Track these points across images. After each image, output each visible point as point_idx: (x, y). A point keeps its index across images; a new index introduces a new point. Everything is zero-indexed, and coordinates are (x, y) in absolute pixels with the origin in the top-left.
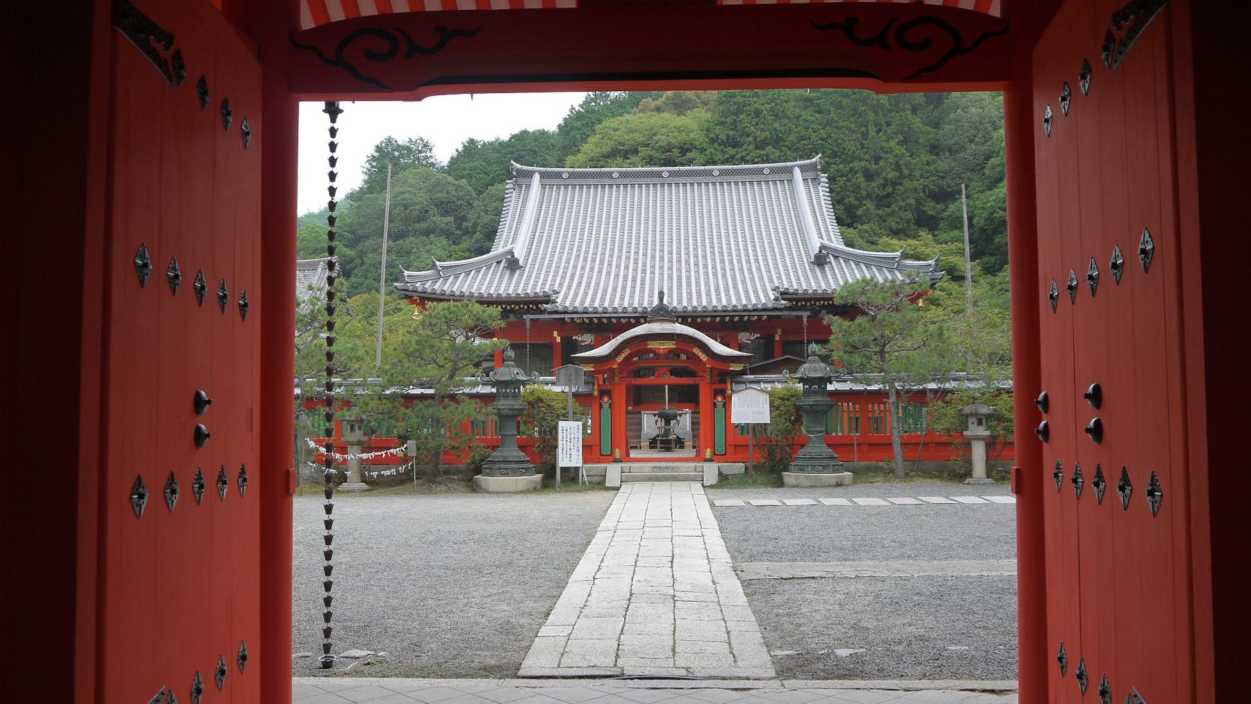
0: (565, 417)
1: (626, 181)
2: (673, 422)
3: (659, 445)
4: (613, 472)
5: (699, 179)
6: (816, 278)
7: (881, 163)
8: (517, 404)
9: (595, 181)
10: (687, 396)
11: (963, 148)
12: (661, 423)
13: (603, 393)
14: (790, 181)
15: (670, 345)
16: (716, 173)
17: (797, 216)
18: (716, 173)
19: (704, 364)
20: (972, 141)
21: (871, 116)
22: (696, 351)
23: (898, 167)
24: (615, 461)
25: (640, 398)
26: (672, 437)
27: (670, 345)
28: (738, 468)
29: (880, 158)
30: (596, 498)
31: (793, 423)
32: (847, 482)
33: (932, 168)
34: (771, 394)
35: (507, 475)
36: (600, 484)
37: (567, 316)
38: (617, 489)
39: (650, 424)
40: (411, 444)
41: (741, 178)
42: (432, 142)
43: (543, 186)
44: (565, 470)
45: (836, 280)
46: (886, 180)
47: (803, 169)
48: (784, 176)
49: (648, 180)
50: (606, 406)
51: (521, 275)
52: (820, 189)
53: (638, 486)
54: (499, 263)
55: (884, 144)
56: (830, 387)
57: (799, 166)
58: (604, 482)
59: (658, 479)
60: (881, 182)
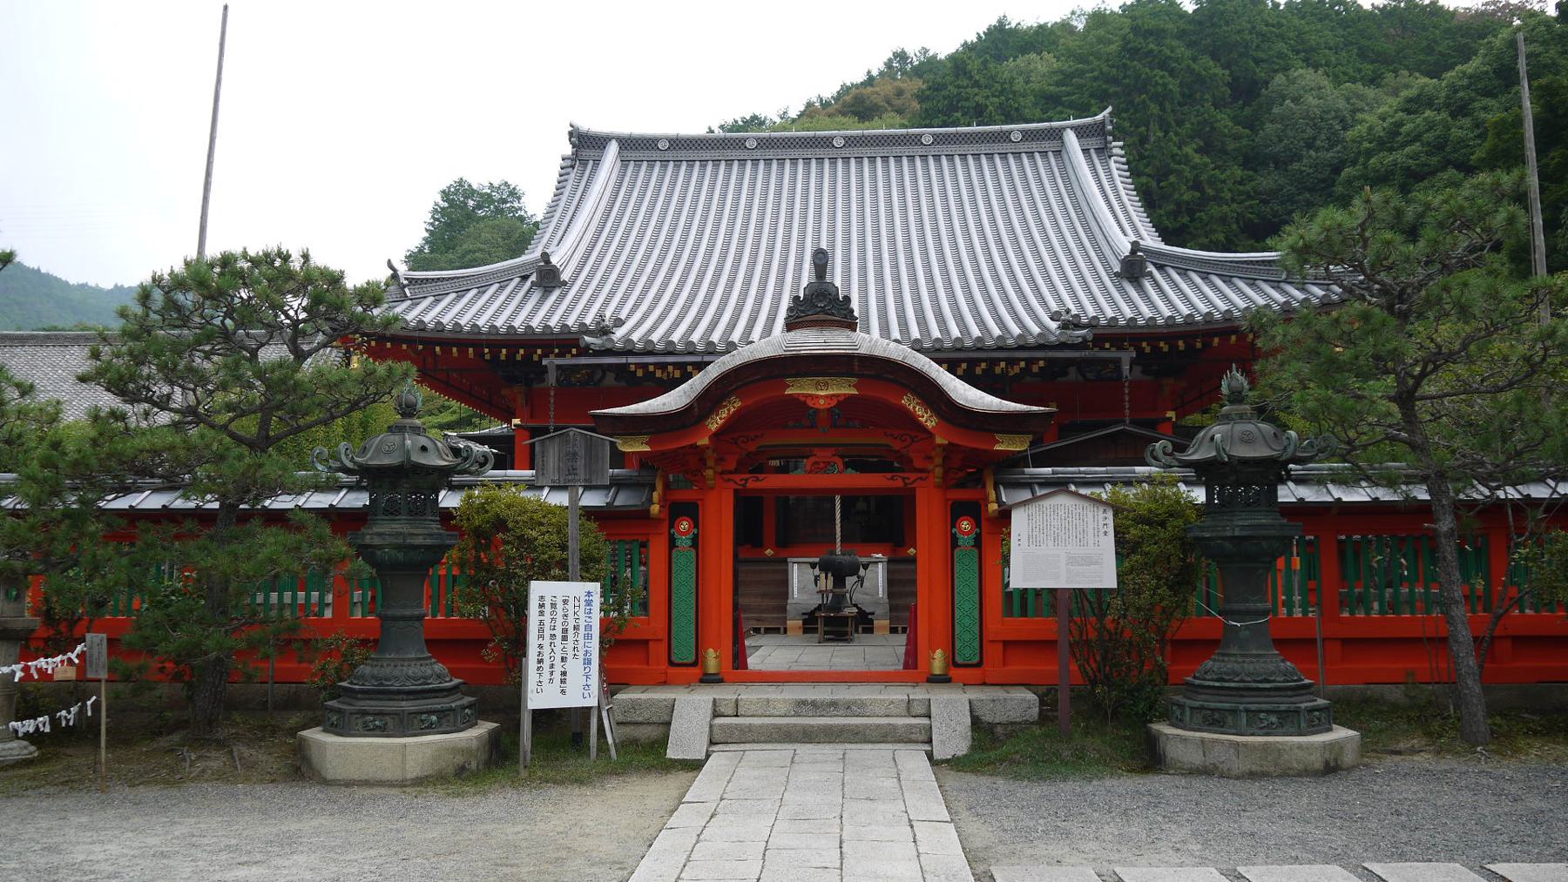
0: (555, 569)
1: (770, 154)
2: (850, 581)
3: (820, 625)
4: (691, 712)
5: (898, 150)
6: (1129, 300)
7: (1172, 179)
8: (423, 533)
9: (716, 154)
10: (884, 524)
11: (1297, 157)
12: (827, 582)
13: (677, 510)
14: (1058, 153)
15: (843, 388)
16: (927, 140)
17: (1077, 207)
18: (927, 140)
19: (929, 434)
20: (1310, 145)
21: (1154, 109)
22: (911, 403)
23: (1197, 186)
24: (708, 680)
25: (769, 529)
26: (850, 611)
27: (843, 388)
28: (1020, 702)
29: (1171, 172)
30: (635, 796)
31: (1174, 587)
32: (1349, 758)
33: (1248, 188)
34: (1118, 509)
35: (383, 731)
36: (648, 753)
37: (632, 360)
38: (695, 766)
39: (803, 583)
40: (95, 642)
41: (974, 149)
42: (521, 188)
43: (625, 163)
44: (545, 718)
45: (1187, 297)
46: (1178, 204)
47: (1081, 132)
48: (1047, 145)
49: (808, 153)
50: (684, 541)
51: (562, 297)
52: (1113, 166)
53: (757, 754)
54: (525, 278)
55: (1176, 150)
56: (1287, 493)
57: (1072, 128)
58: (663, 742)
59: (808, 736)
60: (1172, 207)
